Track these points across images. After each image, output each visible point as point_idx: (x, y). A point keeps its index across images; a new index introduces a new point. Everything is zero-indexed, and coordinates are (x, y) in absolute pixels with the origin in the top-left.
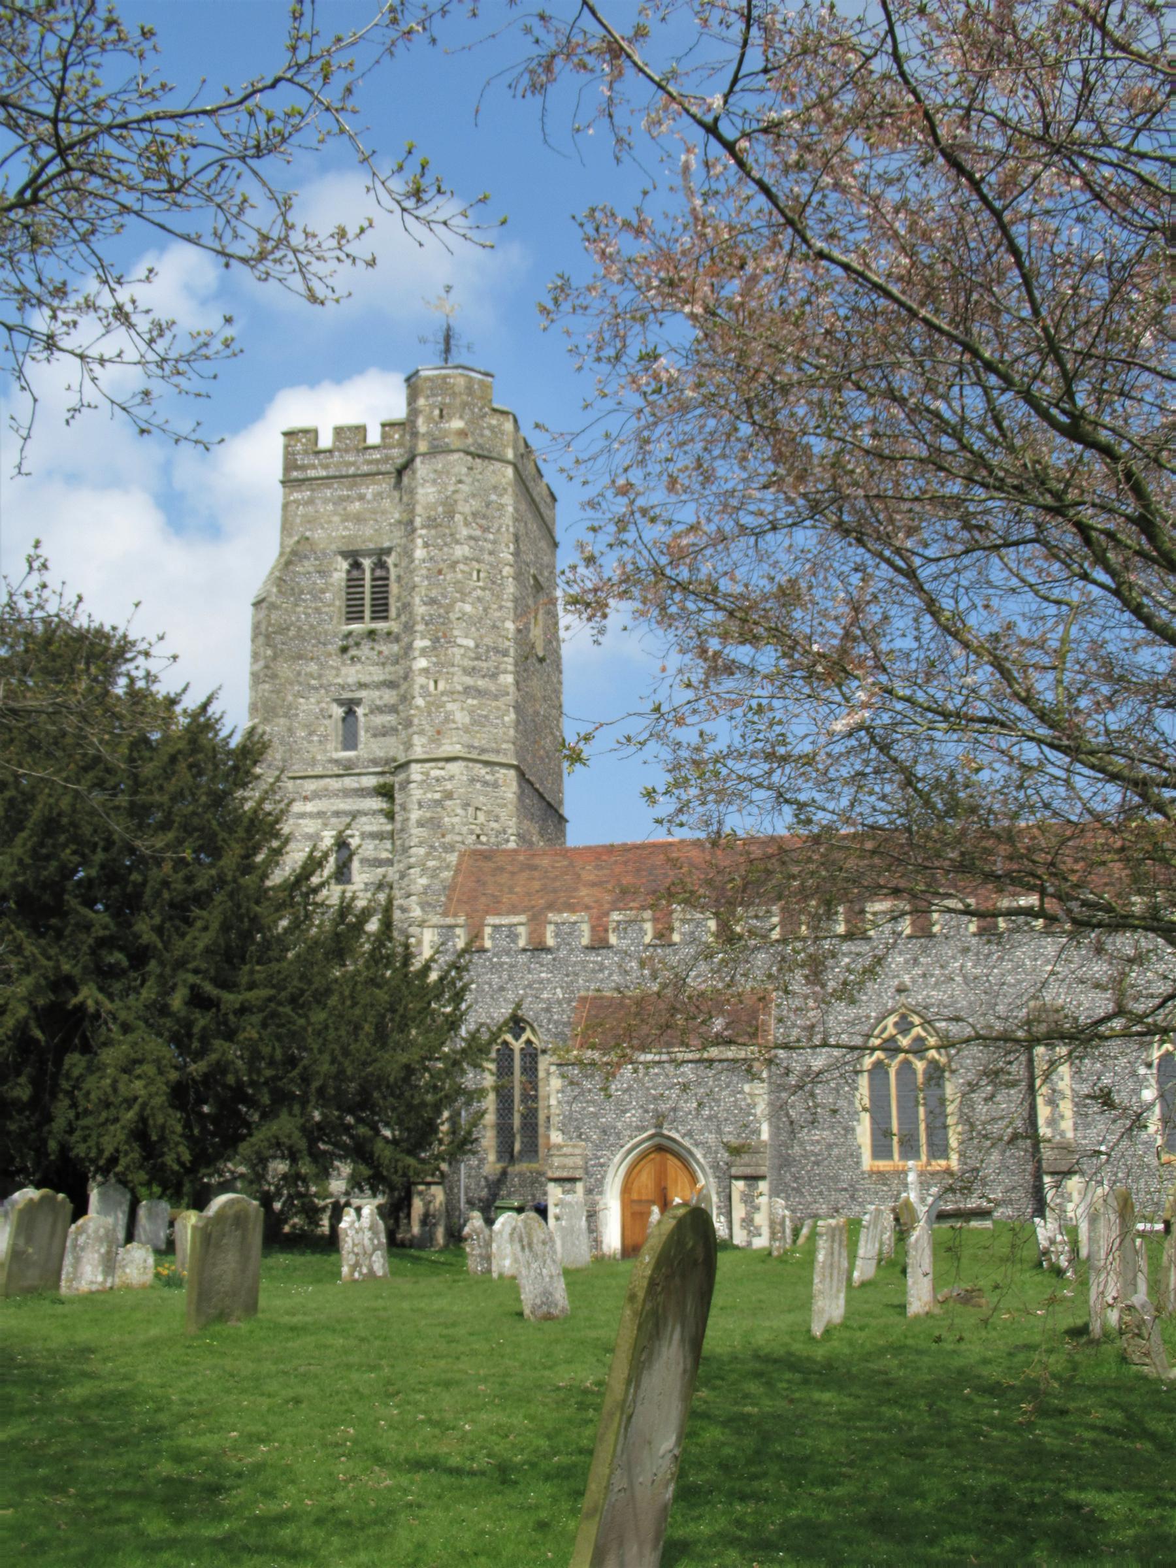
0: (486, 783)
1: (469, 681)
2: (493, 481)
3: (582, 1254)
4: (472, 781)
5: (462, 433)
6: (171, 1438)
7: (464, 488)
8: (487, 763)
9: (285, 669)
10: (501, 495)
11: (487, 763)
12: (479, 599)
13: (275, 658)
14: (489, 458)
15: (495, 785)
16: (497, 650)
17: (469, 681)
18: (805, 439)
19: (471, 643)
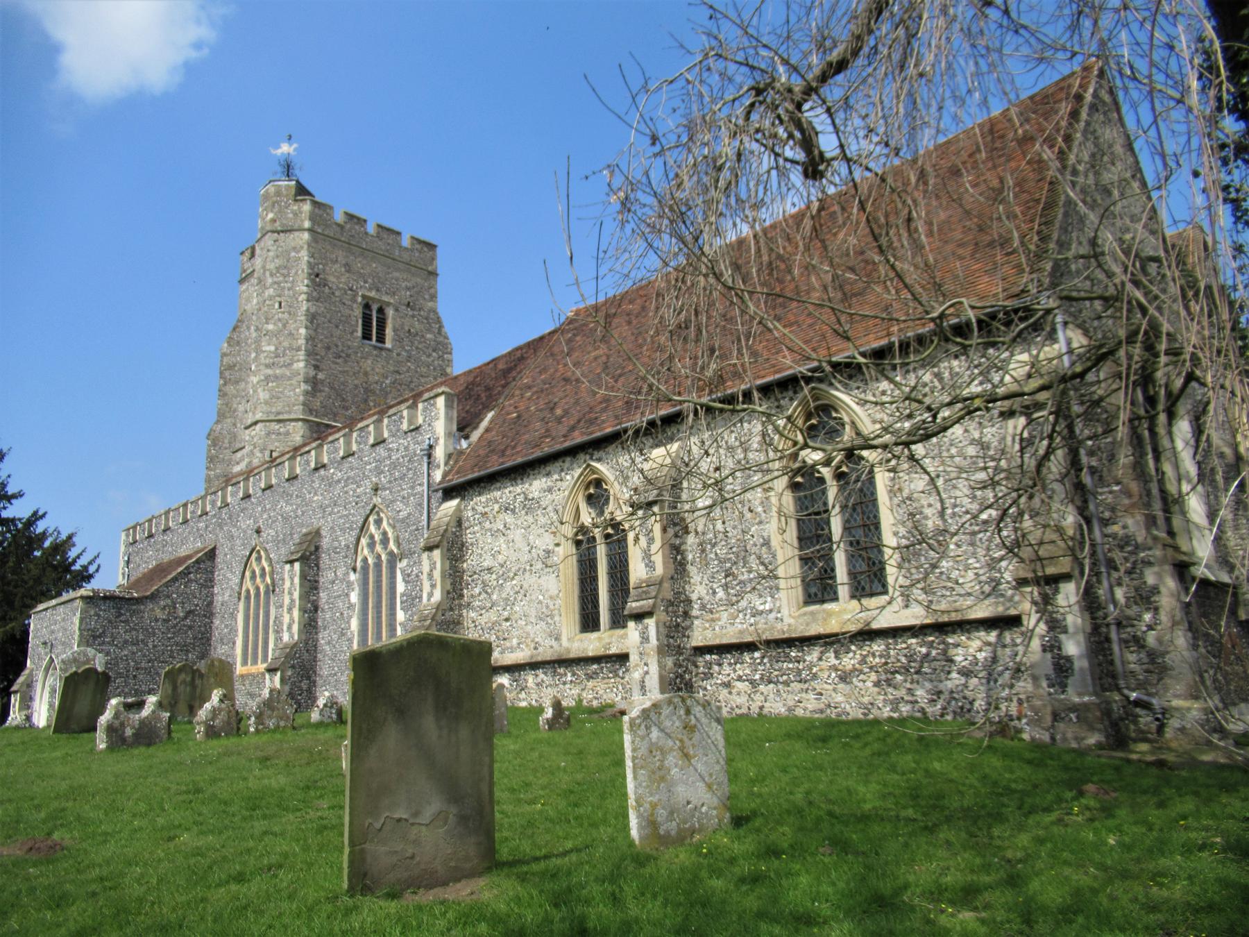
0: (279, 434)
1: (269, 372)
2: (293, 244)
3: (498, 658)
4: (268, 434)
5: (274, 221)
6: (1065, 324)
7: (271, 254)
8: (279, 421)
9: (230, 389)
10: (298, 252)
11: (279, 421)
12: (279, 320)
13: (225, 384)
14: (290, 231)
15: (287, 433)
16: (290, 348)
17: (269, 372)
18: (1012, 723)
19: (272, 348)
